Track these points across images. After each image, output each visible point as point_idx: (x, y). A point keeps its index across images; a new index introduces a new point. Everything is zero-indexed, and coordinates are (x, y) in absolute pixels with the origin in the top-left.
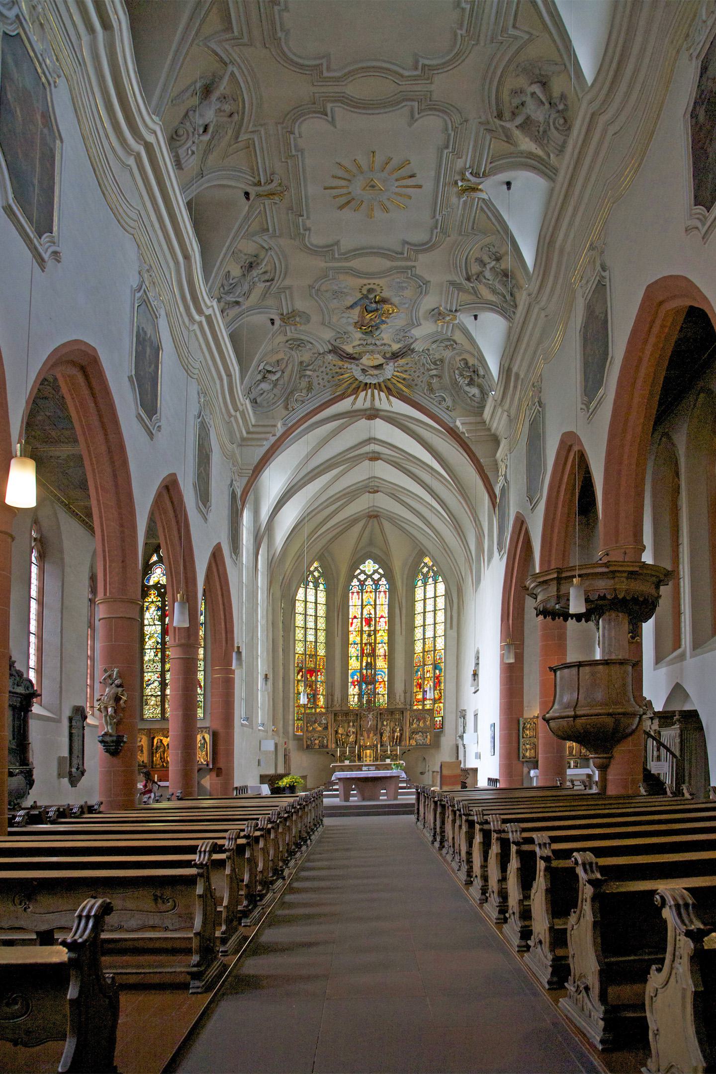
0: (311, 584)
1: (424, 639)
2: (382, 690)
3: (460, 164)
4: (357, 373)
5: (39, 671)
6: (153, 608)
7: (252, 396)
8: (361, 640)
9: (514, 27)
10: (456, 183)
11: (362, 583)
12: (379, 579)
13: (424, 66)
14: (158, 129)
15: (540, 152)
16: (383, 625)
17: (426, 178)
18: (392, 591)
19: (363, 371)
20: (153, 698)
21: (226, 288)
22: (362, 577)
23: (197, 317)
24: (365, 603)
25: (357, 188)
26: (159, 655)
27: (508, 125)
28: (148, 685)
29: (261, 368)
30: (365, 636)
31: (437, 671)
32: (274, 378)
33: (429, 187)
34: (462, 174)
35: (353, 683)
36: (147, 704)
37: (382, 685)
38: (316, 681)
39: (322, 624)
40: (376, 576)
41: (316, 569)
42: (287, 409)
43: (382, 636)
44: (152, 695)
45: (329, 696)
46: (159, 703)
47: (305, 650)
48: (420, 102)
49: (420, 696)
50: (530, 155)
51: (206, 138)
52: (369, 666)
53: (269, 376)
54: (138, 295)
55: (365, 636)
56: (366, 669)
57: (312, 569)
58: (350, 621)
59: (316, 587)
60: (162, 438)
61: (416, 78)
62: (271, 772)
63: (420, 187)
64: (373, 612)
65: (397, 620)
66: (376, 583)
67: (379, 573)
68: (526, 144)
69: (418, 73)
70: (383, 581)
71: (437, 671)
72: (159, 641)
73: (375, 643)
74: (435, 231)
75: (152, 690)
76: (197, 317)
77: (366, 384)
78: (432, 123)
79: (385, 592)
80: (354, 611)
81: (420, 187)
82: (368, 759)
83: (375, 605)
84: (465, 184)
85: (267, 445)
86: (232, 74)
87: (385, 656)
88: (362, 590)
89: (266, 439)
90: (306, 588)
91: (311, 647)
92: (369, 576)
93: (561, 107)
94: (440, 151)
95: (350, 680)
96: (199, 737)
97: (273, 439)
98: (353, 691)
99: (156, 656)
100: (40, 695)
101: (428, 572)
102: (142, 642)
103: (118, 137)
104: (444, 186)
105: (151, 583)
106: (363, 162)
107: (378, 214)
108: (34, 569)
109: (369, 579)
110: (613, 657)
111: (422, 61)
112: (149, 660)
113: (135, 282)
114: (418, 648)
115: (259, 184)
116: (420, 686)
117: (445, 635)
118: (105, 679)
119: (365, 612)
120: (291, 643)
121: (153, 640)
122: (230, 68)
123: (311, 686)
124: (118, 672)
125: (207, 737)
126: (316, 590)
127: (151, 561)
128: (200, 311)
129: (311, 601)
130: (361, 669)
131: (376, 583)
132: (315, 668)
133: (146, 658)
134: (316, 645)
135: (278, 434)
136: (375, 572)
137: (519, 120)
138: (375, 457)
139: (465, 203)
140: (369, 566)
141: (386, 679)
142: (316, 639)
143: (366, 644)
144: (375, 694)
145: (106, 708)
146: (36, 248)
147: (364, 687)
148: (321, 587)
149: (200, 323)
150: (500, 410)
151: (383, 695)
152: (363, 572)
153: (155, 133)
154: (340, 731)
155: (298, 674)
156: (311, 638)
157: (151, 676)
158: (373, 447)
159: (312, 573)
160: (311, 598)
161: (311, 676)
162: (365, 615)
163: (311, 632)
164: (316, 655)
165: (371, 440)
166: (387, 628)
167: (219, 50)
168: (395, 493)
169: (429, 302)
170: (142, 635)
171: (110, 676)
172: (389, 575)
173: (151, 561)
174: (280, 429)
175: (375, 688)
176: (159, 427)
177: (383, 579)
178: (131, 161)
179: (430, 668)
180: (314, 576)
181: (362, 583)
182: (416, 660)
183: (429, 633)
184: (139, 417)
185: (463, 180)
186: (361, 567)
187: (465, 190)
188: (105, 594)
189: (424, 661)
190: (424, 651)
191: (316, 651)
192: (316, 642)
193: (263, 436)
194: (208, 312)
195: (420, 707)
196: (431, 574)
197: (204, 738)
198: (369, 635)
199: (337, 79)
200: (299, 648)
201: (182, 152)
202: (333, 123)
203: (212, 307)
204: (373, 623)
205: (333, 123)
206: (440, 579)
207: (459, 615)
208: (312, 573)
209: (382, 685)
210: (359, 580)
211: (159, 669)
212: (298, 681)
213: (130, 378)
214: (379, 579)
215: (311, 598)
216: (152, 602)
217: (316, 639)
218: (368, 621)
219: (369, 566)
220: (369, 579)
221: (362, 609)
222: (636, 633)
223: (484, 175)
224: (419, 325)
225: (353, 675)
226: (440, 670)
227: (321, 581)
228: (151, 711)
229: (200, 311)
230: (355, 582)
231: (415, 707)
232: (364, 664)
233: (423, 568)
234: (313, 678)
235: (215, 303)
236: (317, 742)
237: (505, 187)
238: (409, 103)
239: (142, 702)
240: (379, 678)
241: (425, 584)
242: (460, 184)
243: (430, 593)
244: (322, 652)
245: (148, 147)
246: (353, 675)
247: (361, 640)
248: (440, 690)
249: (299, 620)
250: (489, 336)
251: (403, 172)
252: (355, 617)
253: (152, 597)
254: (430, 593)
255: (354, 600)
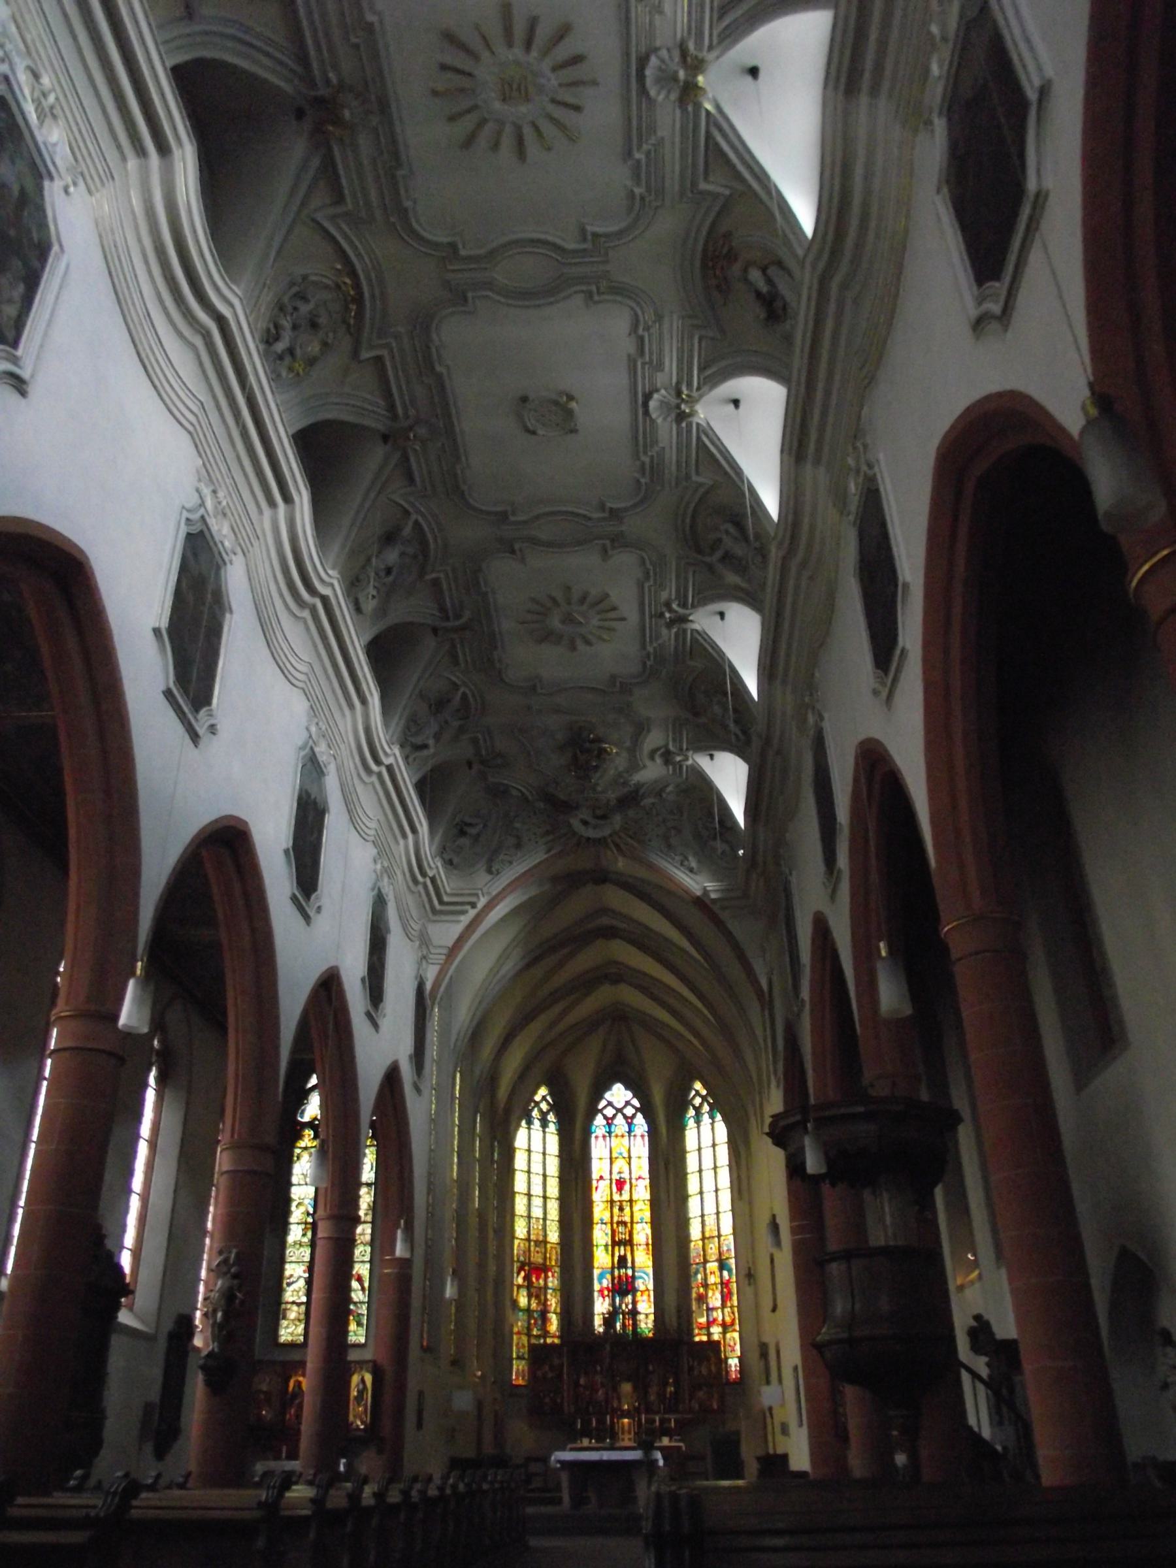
0: (537, 1124)
1: (703, 1216)
2: (646, 1307)
3: (664, 595)
4: (576, 823)
5: (137, 1254)
6: (305, 1157)
7: (447, 857)
8: (612, 1217)
9: (706, 179)
10: (662, 615)
11: (609, 1121)
12: (634, 1116)
13: (611, 509)
14: (336, 583)
15: (744, 585)
16: (642, 1192)
17: (629, 609)
18: (653, 1133)
19: (585, 823)
20: (295, 1308)
21: (413, 730)
22: (609, 1112)
23: (374, 767)
24: (614, 1155)
25: (555, 622)
26: (309, 1234)
27: (708, 559)
28: (289, 1284)
29: (457, 820)
30: (616, 1210)
31: (725, 1273)
32: (473, 831)
33: (633, 617)
34: (668, 605)
35: (601, 1291)
36: (284, 1318)
37: (645, 1297)
38: (546, 1287)
39: (553, 1189)
40: (629, 1111)
41: (544, 1098)
42: (489, 871)
43: (643, 1211)
44: (293, 1303)
45: (566, 1316)
46: (302, 1317)
47: (529, 1232)
48: (613, 541)
49: (703, 1320)
50: (737, 588)
51: (391, 578)
52: (622, 1261)
53: (467, 829)
54: (302, 753)
55: (616, 1210)
56: (619, 1268)
57: (537, 1098)
58: (594, 1183)
59: (544, 1124)
60: (322, 923)
61: (604, 519)
62: (470, 1453)
63: (623, 619)
64: (626, 1169)
65: (662, 1181)
66: (629, 1120)
67: (633, 1107)
68: (732, 578)
69: (606, 515)
70: (640, 1119)
71: (725, 1273)
72: (311, 1210)
73: (632, 1222)
74: (646, 585)
75: (294, 1292)
76: (374, 767)
77: (588, 839)
78: (626, 560)
79: (642, 1136)
80: (599, 1167)
81: (623, 619)
82: (627, 1437)
83: (630, 1157)
84: (673, 615)
85: (465, 920)
86: (416, 523)
87: (647, 1244)
88: (610, 1133)
89: (464, 912)
90: (529, 1128)
91: (537, 1226)
92: (619, 1110)
93: (757, 545)
94: (641, 586)
95: (597, 1287)
96: (355, 1379)
97: (472, 913)
98: (601, 1306)
99: (304, 1235)
100: (132, 1292)
101: (701, 1105)
102: (287, 1213)
103: (293, 595)
104: (651, 617)
105: (306, 1118)
106: (559, 595)
107: (579, 644)
108: (150, 1095)
109: (620, 1115)
110: (900, 1243)
111: (609, 505)
112: (295, 1243)
113: (300, 738)
114: (695, 1232)
115: (448, 619)
116: (702, 1299)
117: (733, 1210)
118: (218, 1265)
119: (615, 1170)
120: (508, 1218)
121: (302, 1209)
122: (414, 517)
123: (537, 1297)
124: (237, 1255)
125: (368, 1378)
126: (544, 1132)
127: (309, 1085)
128: (378, 762)
129: (536, 1148)
130: (613, 1268)
131: (629, 1120)
132: (544, 1264)
133: (291, 1239)
134: (545, 1226)
135: (480, 905)
136: (628, 1103)
137: (719, 554)
138: (610, 933)
139: (677, 634)
140: (618, 1094)
141: (651, 1287)
142: (545, 1213)
143: (618, 1223)
144: (634, 1313)
145: (215, 1311)
146: (190, 724)
147: (617, 1300)
148: (552, 1128)
149: (380, 775)
150: (754, 876)
151: (647, 1315)
152: (610, 1104)
153: (332, 585)
154: (582, 1381)
155: (518, 1274)
156: (537, 1212)
157: (295, 1270)
158: (605, 921)
159: (537, 1104)
160: (537, 1146)
161: (538, 1279)
162: (615, 1176)
163: (537, 1202)
164: (545, 1242)
165: (605, 911)
166: (648, 1197)
167: (403, 503)
168: (647, 986)
169: (654, 739)
170: (288, 1200)
171: (225, 1261)
172: (646, 1110)
173: (309, 1085)
174: (482, 902)
175: (634, 1303)
176: (319, 908)
177: (639, 1115)
178: (306, 614)
179: (713, 1266)
180: (540, 1110)
181: (609, 1121)
182: (693, 1254)
183: (710, 1208)
184: (294, 899)
185: (671, 610)
186: (608, 1095)
187: (671, 624)
188: (232, 1136)
189: (704, 1255)
190: (703, 1239)
191: (545, 1236)
192: (545, 1219)
193: (459, 908)
194: (387, 761)
195: (705, 1338)
196: (706, 1108)
197: (363, 1381)
198: (621, 1209)
199: (525, 522)
200: (520, 1230)
201: (362, 599)
202: (523, 560)
203: (393, 755)
204: (627, 1187)
205: (523, 560)
206: (719, 1117)
207: (749, 1178)
208: (537, 1104)
209: (645, 1297)
210: (605, 1117)
211: (307, 1258)
212: (519, 1287)
213: (286, 852)
214: (634, 1116)
215: (537, 1146)
216: (306, 1148)
217: (545, 1213)
218: (620, 1184)
219: (618, 1094)
220: (620, 1115)
221: (611, 1163)
222: (925, 1203)
223: (693, 606)
224: (645, 766)
225: (601, 1276)
226: (730, 1271)
227: (551, 1117)
228: (290, 1330)
229: (378, 762)
230: (599, 1120)
231: (697, 1339)
232: (616, 1259)
233: (694, 1097)
234: (541, 1282)
235: (397, 751)
236: (547, 1400)
237: (718, 617)
238: (601, 542)
239: (276, 1311)
240: (640, 1284)
241: (698, 1122)
242: (667, 615)
243: (706, 1141)
244: (554, 1236)
245: (325, 600)
246: (601, 1276)
247: (612, 1217)
248: (732, 1307)
249: (520, 1183)
250: (730, 777)
251: (601, 606)
252: (601, 1178)
253: (306, 1139)
254: (706, 1141)
255: (598, 1150)
